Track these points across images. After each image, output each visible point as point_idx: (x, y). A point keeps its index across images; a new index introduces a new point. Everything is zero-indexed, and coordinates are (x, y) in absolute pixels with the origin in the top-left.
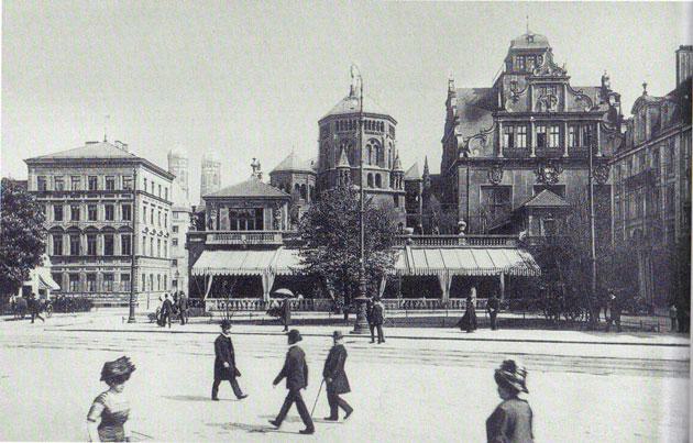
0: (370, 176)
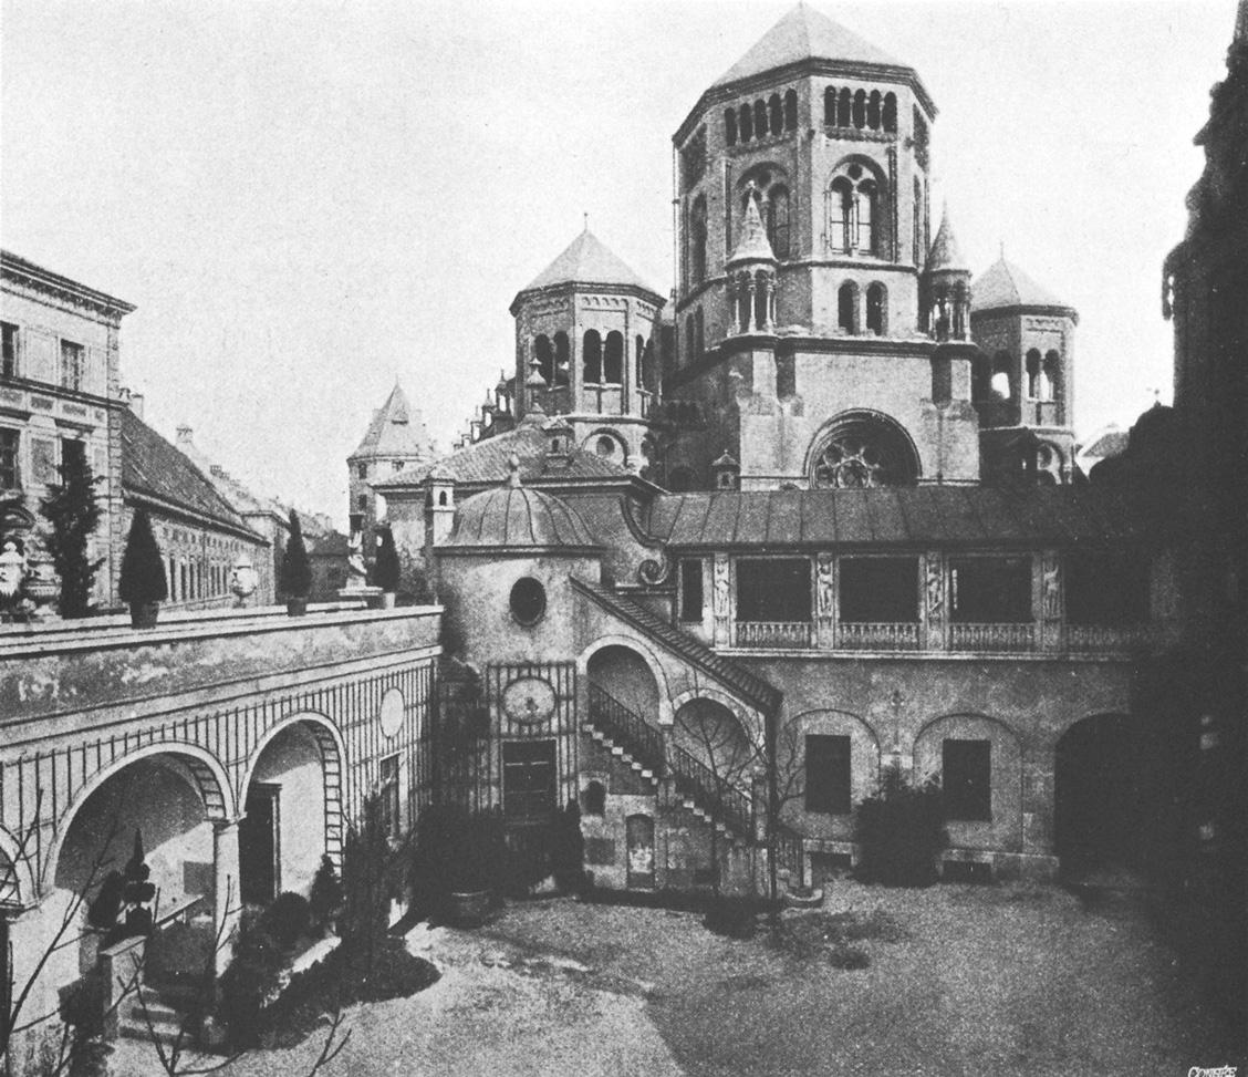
0: (847, 293)
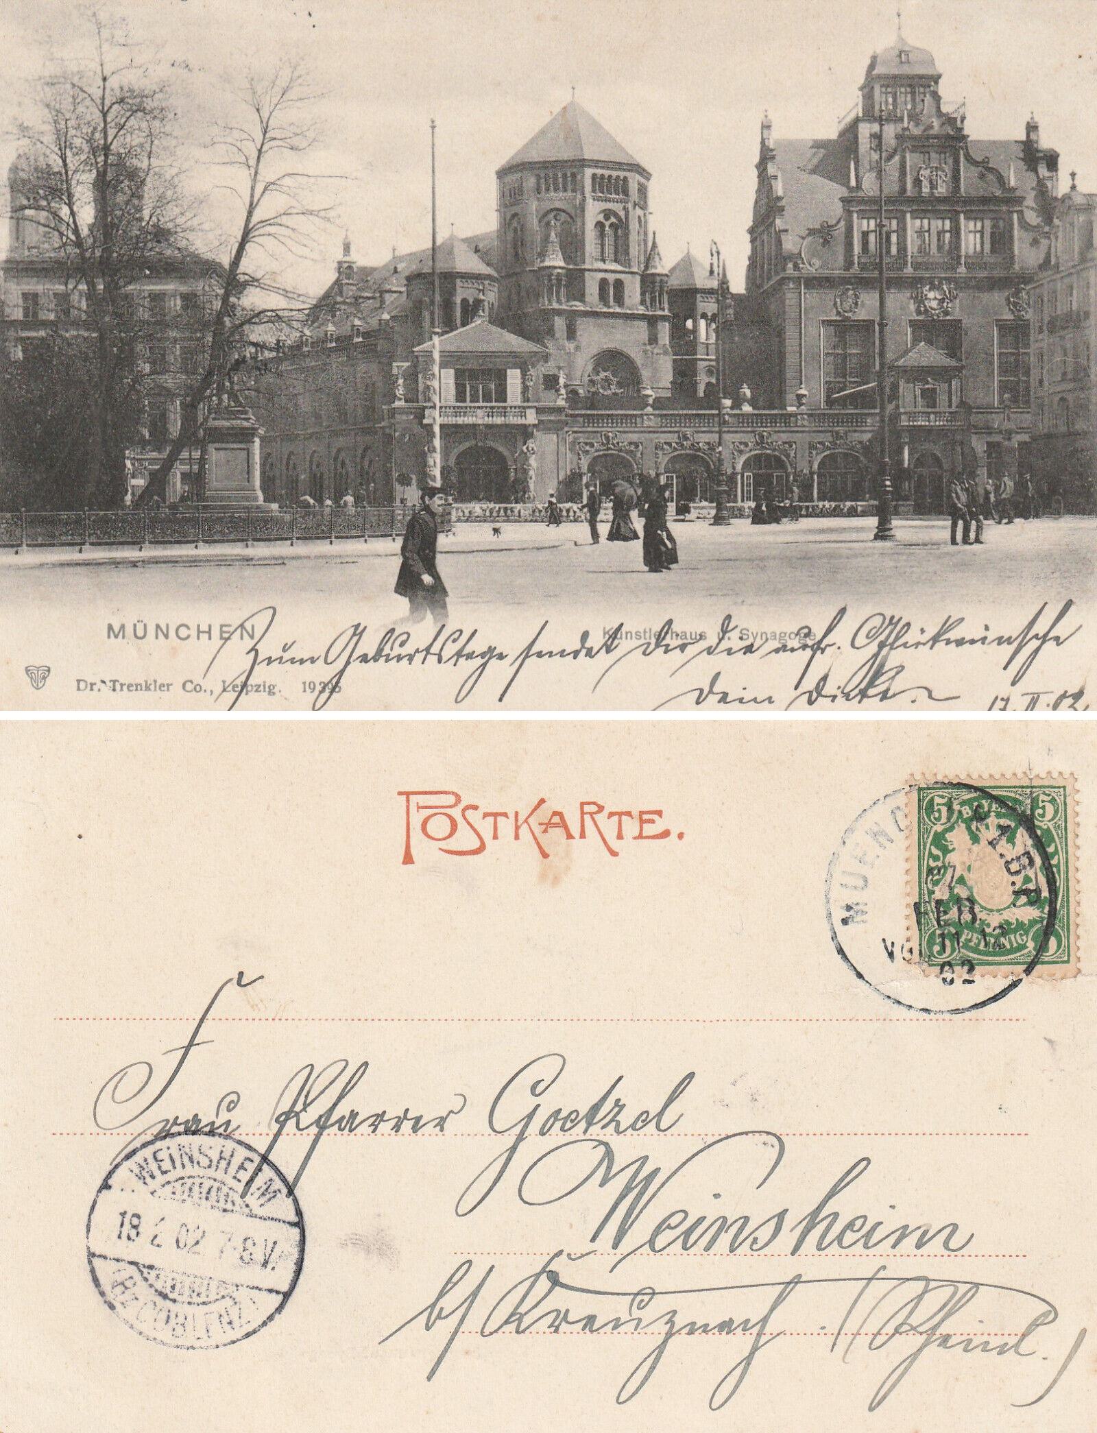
0: (603, 284)
